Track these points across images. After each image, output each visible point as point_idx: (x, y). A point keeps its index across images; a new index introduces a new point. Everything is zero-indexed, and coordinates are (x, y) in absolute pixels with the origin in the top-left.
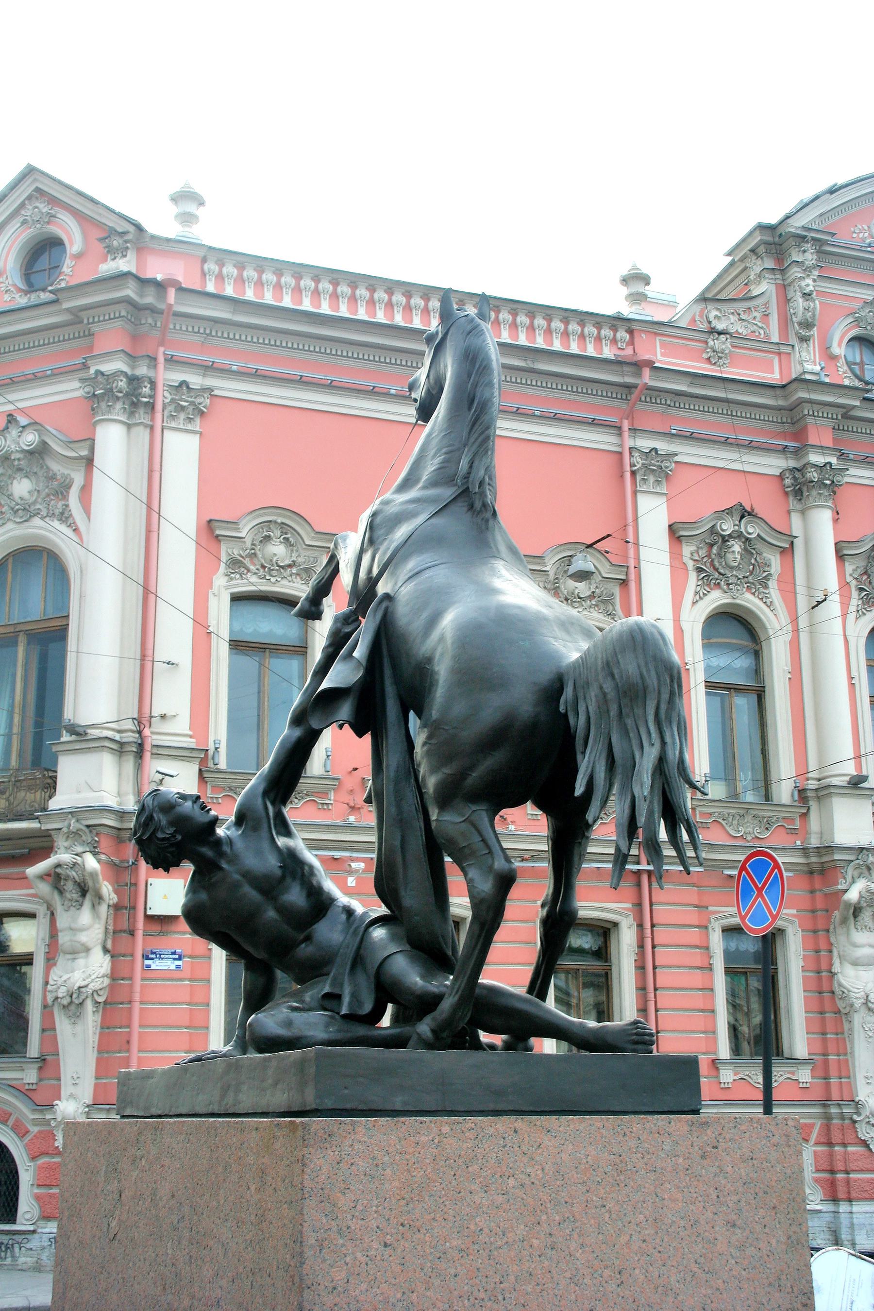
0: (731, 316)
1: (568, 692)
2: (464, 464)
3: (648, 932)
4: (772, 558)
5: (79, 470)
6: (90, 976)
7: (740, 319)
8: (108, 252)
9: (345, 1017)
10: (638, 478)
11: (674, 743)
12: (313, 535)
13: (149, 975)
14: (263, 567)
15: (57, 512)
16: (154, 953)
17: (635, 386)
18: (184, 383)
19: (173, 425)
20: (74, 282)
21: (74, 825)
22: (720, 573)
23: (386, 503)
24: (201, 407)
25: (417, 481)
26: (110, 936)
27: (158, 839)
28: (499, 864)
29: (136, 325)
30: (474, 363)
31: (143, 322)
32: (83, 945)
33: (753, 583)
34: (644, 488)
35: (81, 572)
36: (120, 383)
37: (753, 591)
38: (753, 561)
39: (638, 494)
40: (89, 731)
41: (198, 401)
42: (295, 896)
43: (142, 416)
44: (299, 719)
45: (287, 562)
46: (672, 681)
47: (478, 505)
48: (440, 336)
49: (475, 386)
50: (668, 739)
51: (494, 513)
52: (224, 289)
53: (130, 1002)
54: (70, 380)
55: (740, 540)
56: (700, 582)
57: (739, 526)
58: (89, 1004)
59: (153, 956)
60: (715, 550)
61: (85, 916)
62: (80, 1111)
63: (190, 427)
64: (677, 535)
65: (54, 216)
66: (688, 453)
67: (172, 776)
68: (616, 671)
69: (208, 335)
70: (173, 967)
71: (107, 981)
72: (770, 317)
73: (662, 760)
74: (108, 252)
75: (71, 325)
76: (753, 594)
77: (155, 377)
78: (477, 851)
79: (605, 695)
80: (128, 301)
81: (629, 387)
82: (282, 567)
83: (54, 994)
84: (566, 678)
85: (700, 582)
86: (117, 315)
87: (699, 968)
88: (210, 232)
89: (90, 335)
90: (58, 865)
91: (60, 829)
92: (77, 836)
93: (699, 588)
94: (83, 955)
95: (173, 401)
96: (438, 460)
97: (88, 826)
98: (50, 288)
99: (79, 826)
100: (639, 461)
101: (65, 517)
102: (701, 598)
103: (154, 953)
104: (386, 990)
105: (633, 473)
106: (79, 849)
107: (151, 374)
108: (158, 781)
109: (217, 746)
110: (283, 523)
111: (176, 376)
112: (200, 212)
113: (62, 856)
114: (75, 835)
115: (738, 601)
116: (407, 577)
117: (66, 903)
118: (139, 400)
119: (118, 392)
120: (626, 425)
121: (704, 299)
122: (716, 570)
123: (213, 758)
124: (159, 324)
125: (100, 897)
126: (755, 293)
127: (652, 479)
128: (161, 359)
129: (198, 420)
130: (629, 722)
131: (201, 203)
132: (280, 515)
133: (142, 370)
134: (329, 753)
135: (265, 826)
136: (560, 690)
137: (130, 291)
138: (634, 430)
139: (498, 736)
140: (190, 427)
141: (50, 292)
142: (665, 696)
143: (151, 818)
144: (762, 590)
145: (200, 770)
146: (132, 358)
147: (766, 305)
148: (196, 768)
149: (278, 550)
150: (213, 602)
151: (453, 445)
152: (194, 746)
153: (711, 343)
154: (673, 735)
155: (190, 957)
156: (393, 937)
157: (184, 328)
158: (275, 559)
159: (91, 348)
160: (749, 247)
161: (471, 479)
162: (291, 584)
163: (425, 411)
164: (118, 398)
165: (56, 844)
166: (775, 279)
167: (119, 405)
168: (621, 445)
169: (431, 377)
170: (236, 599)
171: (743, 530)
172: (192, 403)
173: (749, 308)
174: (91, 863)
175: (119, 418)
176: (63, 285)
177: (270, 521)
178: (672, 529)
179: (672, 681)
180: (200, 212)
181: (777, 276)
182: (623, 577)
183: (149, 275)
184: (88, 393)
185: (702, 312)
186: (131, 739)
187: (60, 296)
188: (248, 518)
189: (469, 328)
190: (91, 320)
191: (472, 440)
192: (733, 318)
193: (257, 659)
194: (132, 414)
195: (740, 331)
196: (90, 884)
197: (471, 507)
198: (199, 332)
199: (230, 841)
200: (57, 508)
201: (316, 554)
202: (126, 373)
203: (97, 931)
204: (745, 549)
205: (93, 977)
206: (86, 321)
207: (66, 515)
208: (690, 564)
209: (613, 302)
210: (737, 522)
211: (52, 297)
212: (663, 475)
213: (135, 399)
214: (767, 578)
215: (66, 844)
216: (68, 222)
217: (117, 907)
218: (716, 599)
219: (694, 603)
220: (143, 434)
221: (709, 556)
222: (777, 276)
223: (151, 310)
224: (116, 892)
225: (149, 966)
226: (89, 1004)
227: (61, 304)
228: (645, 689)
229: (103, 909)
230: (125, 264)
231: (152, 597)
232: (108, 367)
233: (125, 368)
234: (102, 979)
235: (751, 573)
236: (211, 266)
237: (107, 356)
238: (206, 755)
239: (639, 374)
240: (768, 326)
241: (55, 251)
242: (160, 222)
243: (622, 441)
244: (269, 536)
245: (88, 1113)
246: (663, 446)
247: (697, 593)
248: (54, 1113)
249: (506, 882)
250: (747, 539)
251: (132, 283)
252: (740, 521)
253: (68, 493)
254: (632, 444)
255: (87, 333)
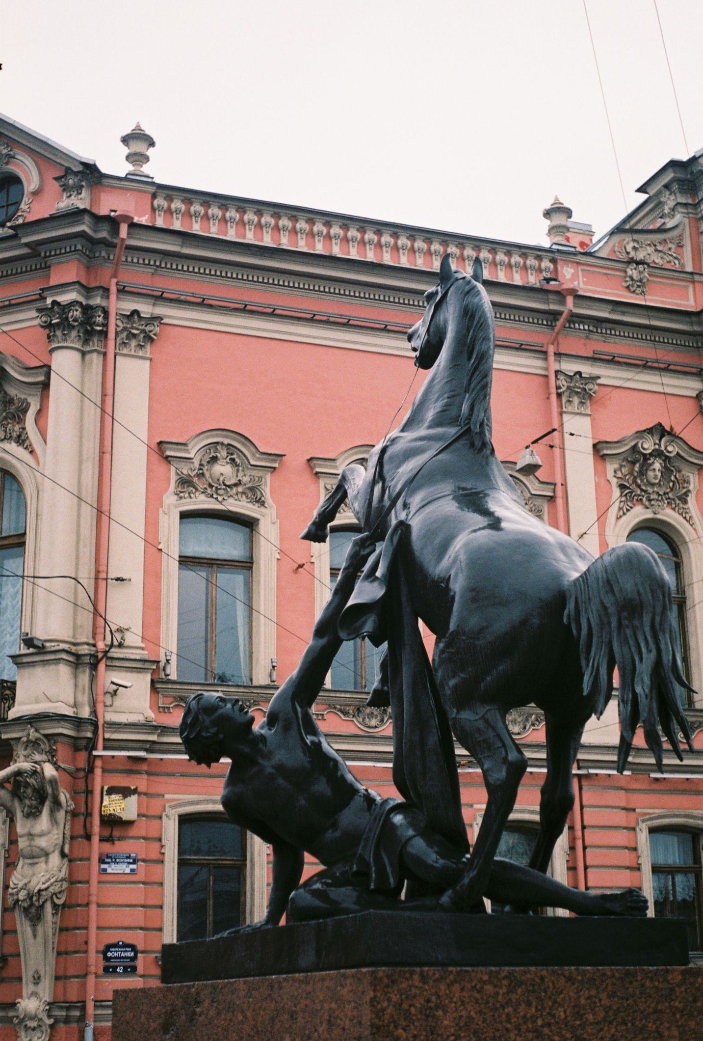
0: (648, 248)
1: (571, 606)
2: (465, 408)
3: (579, 833)
4: (691, 476)
5: (35, 395)
6: (49, 879)
7: (656, 250)
8: (64, 190)
9: (373, 891)
10: (564, 399)
11: (667, 648)
12: (258, 456)
13: (104, 878)
14: (211, 486)
15: (14, 435)
16: (111, 858)
17: (560, 313)
18: (135, 312)
19: (125, 351)
20: (31, 218)
21: (33, 735)
22: (642, 490)
23: (393, 441)
24: (151, 334)
25: (421, 421)
26: (67, 841)
27: (203, 737)
28: (513, 756)
29: (90, 258)
30: (471, 317)
31: (97, 254)
32: (42, 849)
33: (674, 500)
34: (570, 409)
35: (38, 492)
36: (75, 313)
37: (674, 506)
38: (673, 478)
39: (564, 416)
40: (47, 644)
41: (148, 328)
42: (322, 787)
43: (95, 344)
44: (321, 631)
45: (233, 481)
46: (664, 597)
47: (478, 443)
48: (440, 295)
49: (474, 340)
50: (663, 647)
51: (493, 451)
52: (172, 225)
53: (87, 905)
54: (29, 310)
55: (660, 458)
56: (623, 499)
57: (660, 445)
58: (48, 908)
59: (109, 860)
60: (637, 467)
61: (44, 821)
62: (41, 1008)
63: (140, 353)
64: (601, 453)
65: (14, 157)
66: (609, 375)
67: (126, 687)
68: (616, 589)
69: (158, 267)
70: (128, 871)
71: (65, 885)
72: (684, 249)
73: (658, 663)
74: (64, 190)
75: (31, 257)
76: (674, 509)
77: (108, 307)
78: (488, 745)
79: (605, 608)
80: (82, 235)
81: (556, 315)
82: (229, 486)
83: (15, 897)
84: (568, 594)
85: (623, 499)
86: (73, 249)
87: (628, 868)
88: (161, 169)
89: (46, 267)
90: (19, 773)
91: (20, 738)
92: (36, 745)
93: (622, 504)
94: (43, 859)
95: (125, 329)
96: (439, 405)
97: (46, 736)
98: (8, 224)
99: (37, 735)
100: (563, 383)
101: (21, 440)
102: (624, 514)
103: (111, 858)
104: (407, 867)
105: (559, 395)
106: (38, 757)
107: (104, 304)
108: (112, 691)
109: (168, 658)
110: (229, 445)
111: (128, 306)
112: (151, 152)
113: (21, 764)
114: (34, 744)
115: (659, 516)
116: (419, 506)
117: (26, 809)
118: (92, 328)
119: (74, 321)
120: (551, 350)
121: (619, 230)
122: (639, 486)
123: (164, 669)
124: (111, 257)
125: (57, 803)
126: (669, 226)
127: (576, 400)
128: (113, 289)
129: (148, 347)
130: (628, 632)
131: (152, 144)
132: (226, 437)
133: (97, 301)
134: (275, 664)
135: (295, 726)
136: (564, 605)
137: (84, 227)
138: (558, 355)
139: (508, 644)
140: (140, 353)
141: (10, 228)
142: (659, 610)
143: (196, 719)
144: (681, 505)
145: (152, 682)
146: (88, 291)
147: (681, 238)
148: (148, 677)
149: (223, 470)
150: (163, 520)
151: (454, 391)
152: (146, 658)
153: (630, 272)
154: (666, 644)
155: (144, 861)
156: (412, 824)
157: (135, 260)
158: (222, 479)
159: (48, 277)
160: (663, 183)
161: (472, 420)
162: (237, 502)
163: (426, 359)
164: (73, 327)
165: (15, 753)
166: (688, 213)
167: (74, 333)
168: (547, 369)
169: (432, 330)
170: (185, 516)
171: (663, 448)
172: (143, 331)
173: (665, 240)
174: (49, 771)
175: (73, 345)
176: (20, 221)
177: (217, 443)
178: (596, 447)
179: (664, 597)
180: (151, 152)
181: (690, 211)
182: (551, 494)
183: (103, 211)
184: (45, 322)
185: (620, 242)
186: (87, 652)
187: (20, 232)
188: (196, 440)
189: (467, 288)
190: (48, 254)
191: (472, 386)
192: (650, 250)
193: (204, 574)
194: (86, 342)
195: (657, 261)
196: (49, 790)
197: (472, 445)
198: (149, 264)
199: (263, 738)
200: (14, 431)
201: (260, 474)
202: (81, 303)
203: (56, 836)
204: (665, 467)
205: (52, 880)
206: (43, 254)
207: (23, 438)
208: (614, 482)
209: (538, 234)
210: (657, 442)
211: (11, 232)
212: (587, 397)
213: (86, 327)
214: (686, 494)
215: (25, 753)
216: (29, 165)
217: (74, 814)
218: (639, 514)
219: (618, 518)
220: (96, 360)
221: (631, 473)
222: (690, 211)
223: (103, 242)
224: (73, 799)
225: (105, 870)
226: (48, 908)
227: (20, 239)
228: (641, 605)
229: (61, 815)
230: (81, 201)
231: (104, 518)
232: (65, 298)
233: (81, 299)
234: (60, 884)
235: (672, 489)
236: (160, 201)
237: (63, 287)
238: (158, 667)
239: (563, 302)
240: (683, 257)
241: (13, 189)
242: (113, 162)
243: (548, 365)
244: (217, 457)
245: (49, 1011)
246: (587, 369)
247: (620, 509)
248: (17, 1010)
249: (518, 769)
250: (667, 457)
251: (87, 219)
252: (660, 440)
253: (25, 416)
254: (558, 368)
255: (43, 266)
